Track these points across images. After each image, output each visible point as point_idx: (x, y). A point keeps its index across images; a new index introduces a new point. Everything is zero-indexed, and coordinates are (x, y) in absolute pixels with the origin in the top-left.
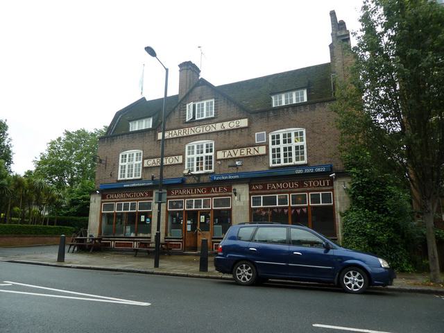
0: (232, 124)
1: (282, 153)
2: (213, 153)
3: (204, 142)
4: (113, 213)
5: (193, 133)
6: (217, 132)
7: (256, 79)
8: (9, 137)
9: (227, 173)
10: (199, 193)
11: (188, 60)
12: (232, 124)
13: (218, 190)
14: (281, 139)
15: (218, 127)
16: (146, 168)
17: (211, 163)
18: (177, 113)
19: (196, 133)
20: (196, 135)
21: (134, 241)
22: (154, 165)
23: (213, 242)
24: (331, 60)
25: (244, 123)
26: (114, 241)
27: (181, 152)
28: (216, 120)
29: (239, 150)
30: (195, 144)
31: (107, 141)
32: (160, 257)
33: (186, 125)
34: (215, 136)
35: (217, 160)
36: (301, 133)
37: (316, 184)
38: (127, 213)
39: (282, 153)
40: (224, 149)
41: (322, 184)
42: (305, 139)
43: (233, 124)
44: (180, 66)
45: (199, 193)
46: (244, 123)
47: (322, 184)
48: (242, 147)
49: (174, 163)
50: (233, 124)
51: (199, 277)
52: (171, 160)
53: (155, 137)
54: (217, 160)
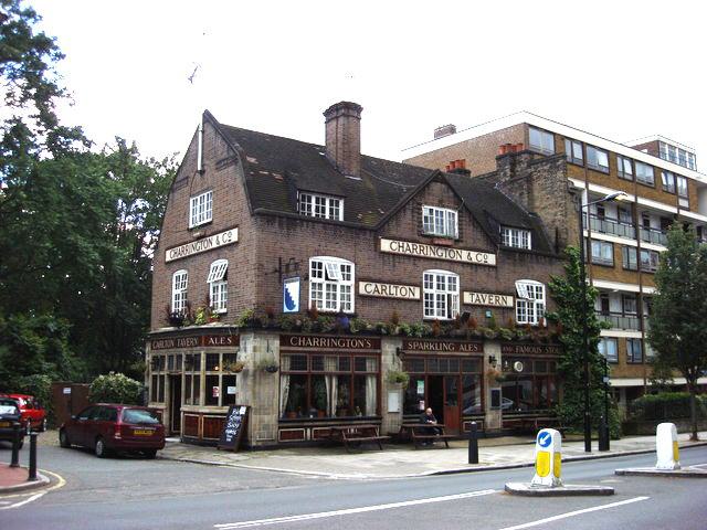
3: (447, 274)
5: (432, 255)
6: (463, 263)
7: (257, 134)
9: (373, 317)
10: (334, 346)
12: (395, 246)
13: (219, 341)
15: (464, 256)
16: (363, 297)
18: (409, 213)
20: (437, 259)
21: (306, 427)
22: (376, 294)
24: (366, 159)
25: (491, 259)
26: (311, 427)
27: (417, 281)
28: (461, 245)
30: (435, 273)
31: (280, 225)
33: (423, 240)
34: (460, 268)
37: (354, 344)
40: (472, 291)
42: (544, 296)
44: (327, 113)
45: (309, 346)
46: (491, 259)
48: (490, 292)
49: (407, 296)
51: (584, 459)
53: (376, 247)
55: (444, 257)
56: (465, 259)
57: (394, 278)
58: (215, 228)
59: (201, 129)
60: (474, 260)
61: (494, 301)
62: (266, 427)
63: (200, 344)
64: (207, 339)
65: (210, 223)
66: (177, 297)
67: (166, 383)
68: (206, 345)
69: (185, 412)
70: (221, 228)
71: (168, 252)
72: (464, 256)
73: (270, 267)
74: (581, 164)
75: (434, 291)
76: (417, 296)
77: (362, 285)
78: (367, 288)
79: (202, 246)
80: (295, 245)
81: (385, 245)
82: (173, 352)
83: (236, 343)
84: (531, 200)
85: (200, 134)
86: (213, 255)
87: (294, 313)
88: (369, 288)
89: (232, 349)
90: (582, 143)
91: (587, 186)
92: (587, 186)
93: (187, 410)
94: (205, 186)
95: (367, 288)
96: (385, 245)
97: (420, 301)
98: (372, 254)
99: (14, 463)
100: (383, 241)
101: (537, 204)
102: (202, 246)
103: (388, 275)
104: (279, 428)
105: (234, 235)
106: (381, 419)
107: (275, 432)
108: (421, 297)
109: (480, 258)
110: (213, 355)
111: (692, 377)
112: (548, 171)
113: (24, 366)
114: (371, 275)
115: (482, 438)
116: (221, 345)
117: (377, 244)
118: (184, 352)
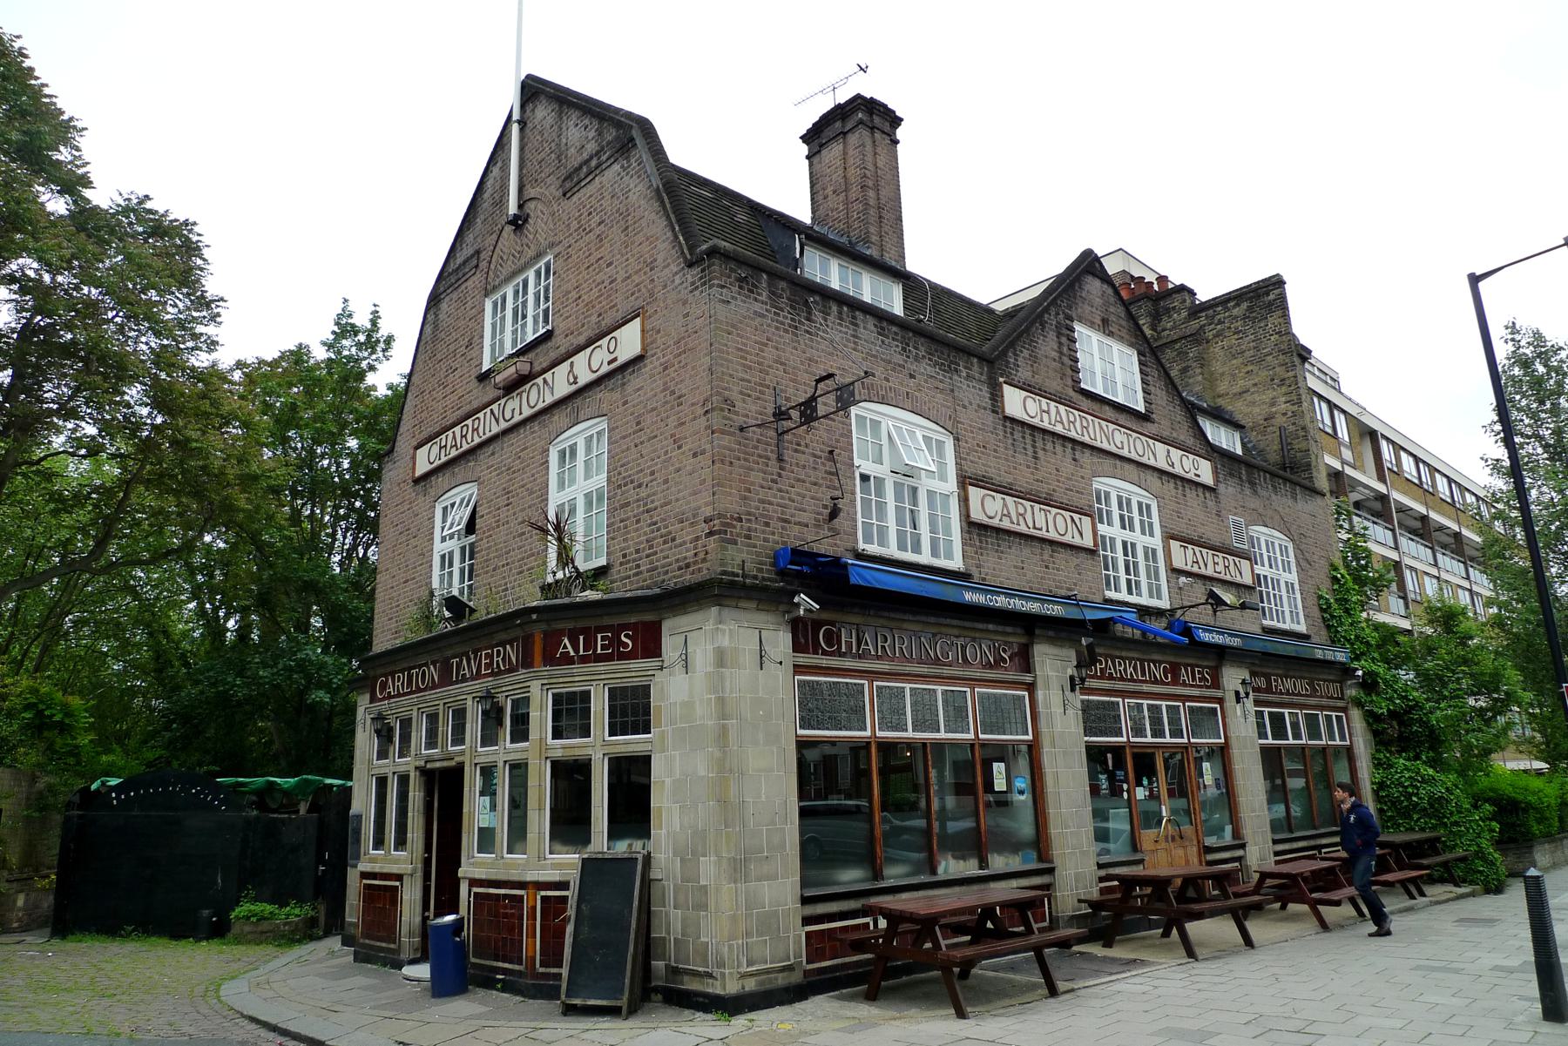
3: (1137, 494)
12: (1033, 407)
34: (1153, 480)
44: (806, 138)
57: (1035, 487)
58: (561, 343)
59: (516, 116)
61: (1220, 568)
62: (768, 924)
63: (527, 662)
64: (552, 641)
65: (548, 335)
66: (447, 560)
67: (416, 795)
68: (550, 659)
69: (474, 882)
70: (582, 340)
71: (422, 453)
73: (754, 409)
77: (975, 494)
78: (989, 507)
79: (518, 407)
81: (1015, 402)
82: (438, 698)
83: (650, 646)
84: (1211, 380)
85: (515, 128)
86: (558, 418)
89: (633, 671)
93: (480, 874)
94: (531, 253)
95: (989, 507)
96: (1015, 402)
98: (990, 418)
99: (1513, 328)
100: (1008, 391)
101: (1222, 387)
102: (518, 407)
103: (1024, 479)
104: (807, 921)
105: (629, 341)
106: (1051, 871)
107: (795, 937)
108: (1096, 544)
109: (1187, 464)
110: (572, 696)
112: (1245, 317)
113: (51, 772)
114: (992, 473)
116: (599, 659)
117: (996, 397)
118: (468, 694)
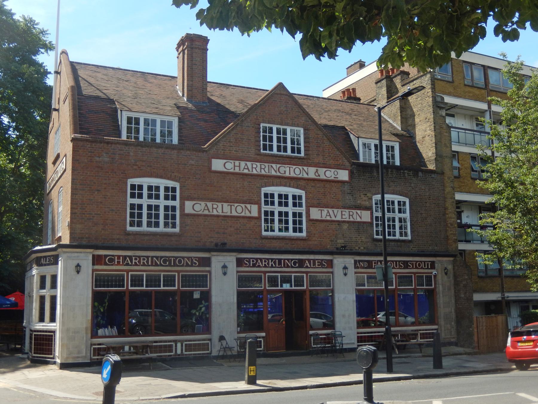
0: (328, 174)
1: (145, 211)
2: (304, 207)
3: (291, 191)
4: (124, 292)
8: (429, 124)
11: (184, 35)
14: (145, 192)
17: (174, 217)
19: (278, 174)
22: (206, 212)
23: (92, 345)
25: (344, 175)
27: (367, 203)
29: (340, 210)
30: (276, 190)
32: (122, 374)
35: (183, 215)
36: (174, 189)
38: (157, 292)
39: (145, 211)
40: (320, 205)
41: (425, 266)
43: (330, 174)
47: (425, 266)
50: (330, 174)
52: (239, 209)
54: (310, 221)
55: (287, 174)
56: (312, 175)
60: (323, 177)
72: (311, 172)
74: (484, 87)
75: (277, 209)
76: (255, 214)
80: (418, 184)
87: (261, 232)
88: (197, 207)
90: (483, 66)
91: (489, 107)
92: (489, 107)
97: (371, 223)
109: (328, 174)
111: (15, 347)
115: (443, 346)
